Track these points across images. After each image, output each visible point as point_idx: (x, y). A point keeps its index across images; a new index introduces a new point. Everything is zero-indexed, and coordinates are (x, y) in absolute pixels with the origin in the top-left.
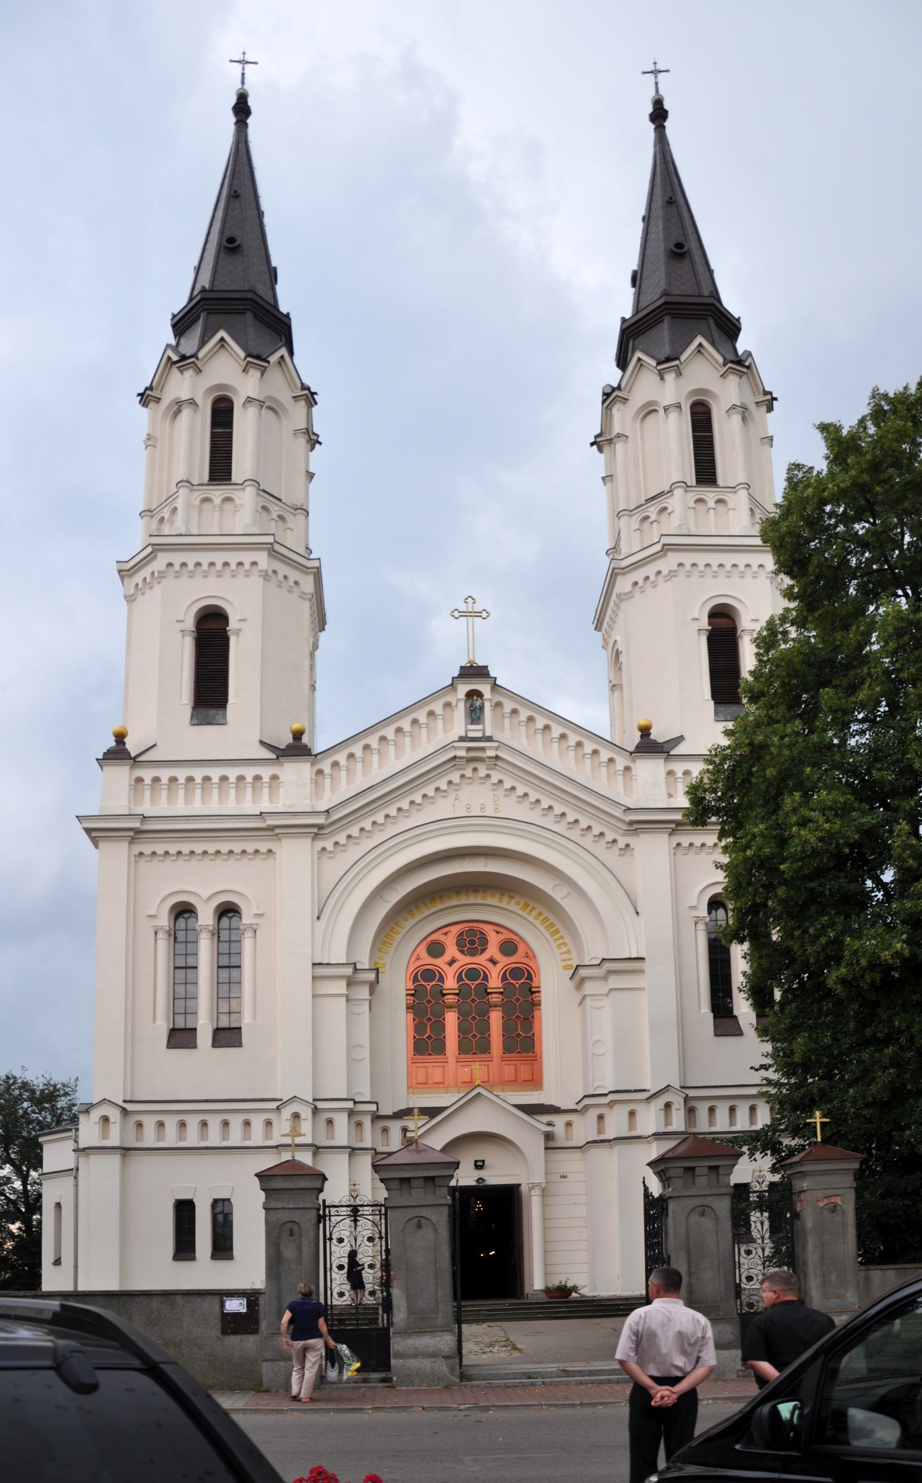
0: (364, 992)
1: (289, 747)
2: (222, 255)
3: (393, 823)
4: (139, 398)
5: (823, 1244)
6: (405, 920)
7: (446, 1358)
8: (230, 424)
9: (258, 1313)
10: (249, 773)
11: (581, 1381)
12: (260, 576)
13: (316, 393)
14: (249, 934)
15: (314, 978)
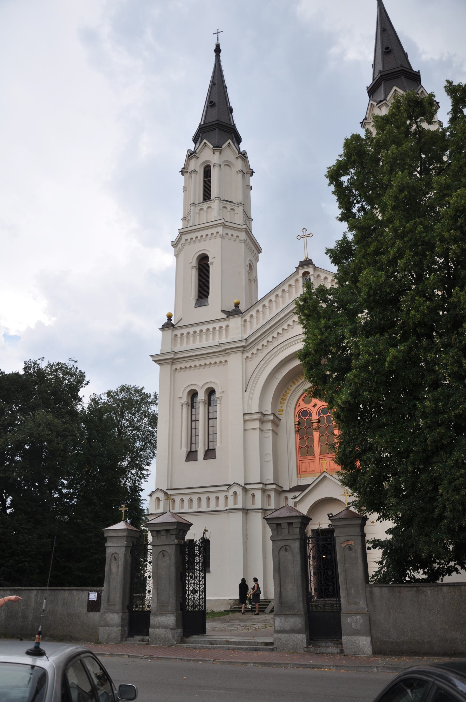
0: (269, 426)
1: (233, 311)
2: (209, 109)
3: (276, 340)
4: (181, 173)
5: (346, 570)
6: (291, 386)
7: (171, 629)
8: (210, 176)
9: (101, 600)
10: (217, 325)
11: (229, 647)
12: (220, 237)
13: (439, 103)
14: (218, 402)
15: (245, 421)
